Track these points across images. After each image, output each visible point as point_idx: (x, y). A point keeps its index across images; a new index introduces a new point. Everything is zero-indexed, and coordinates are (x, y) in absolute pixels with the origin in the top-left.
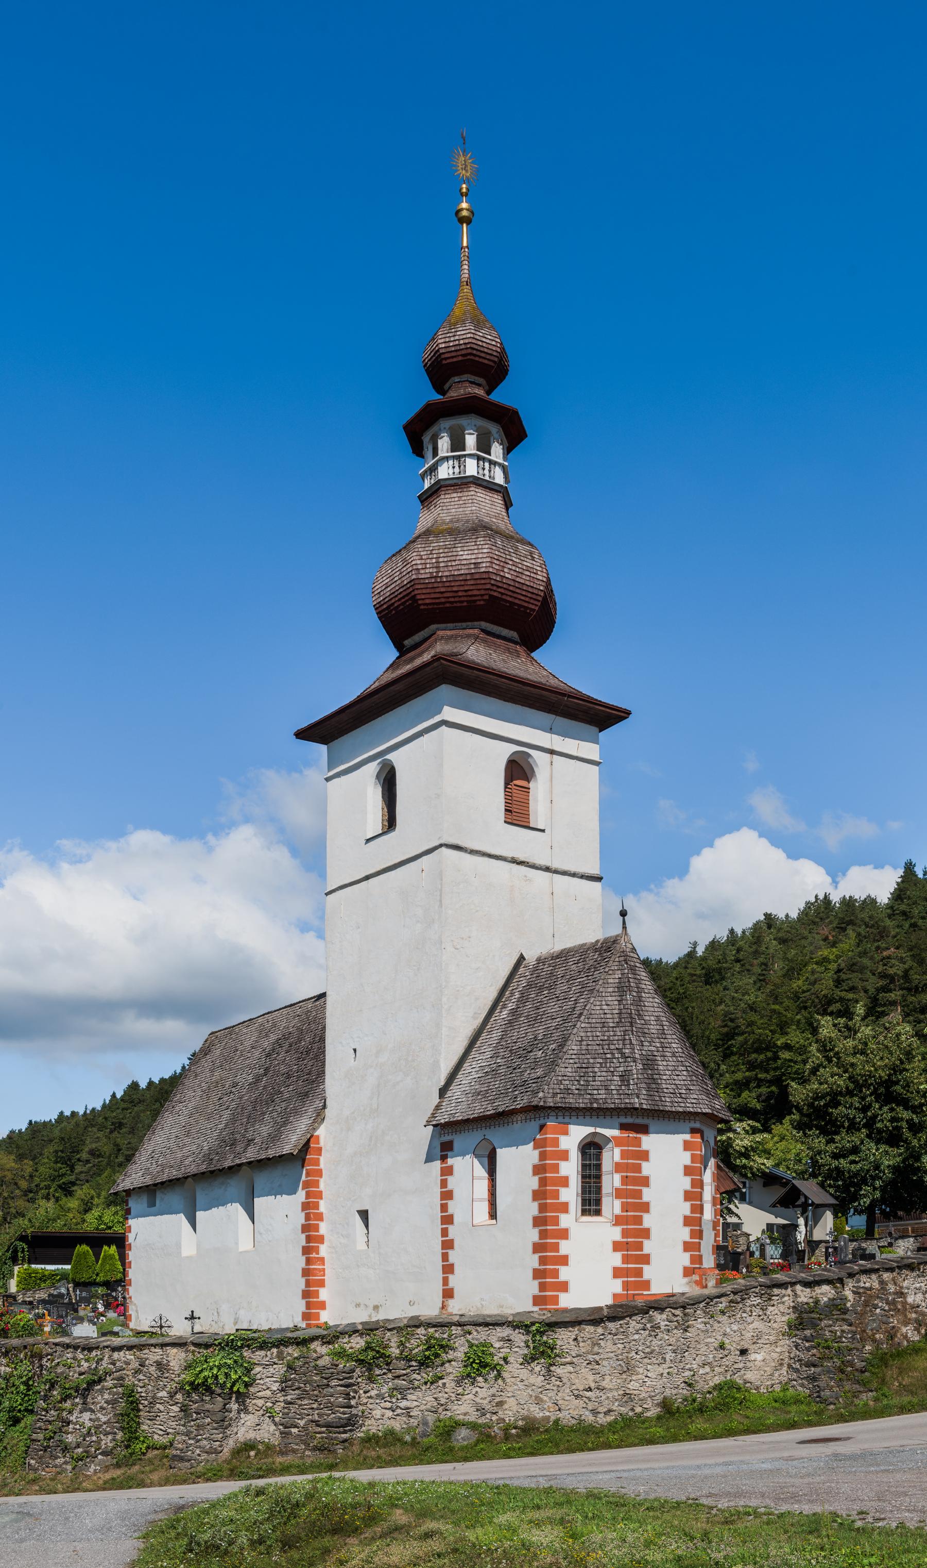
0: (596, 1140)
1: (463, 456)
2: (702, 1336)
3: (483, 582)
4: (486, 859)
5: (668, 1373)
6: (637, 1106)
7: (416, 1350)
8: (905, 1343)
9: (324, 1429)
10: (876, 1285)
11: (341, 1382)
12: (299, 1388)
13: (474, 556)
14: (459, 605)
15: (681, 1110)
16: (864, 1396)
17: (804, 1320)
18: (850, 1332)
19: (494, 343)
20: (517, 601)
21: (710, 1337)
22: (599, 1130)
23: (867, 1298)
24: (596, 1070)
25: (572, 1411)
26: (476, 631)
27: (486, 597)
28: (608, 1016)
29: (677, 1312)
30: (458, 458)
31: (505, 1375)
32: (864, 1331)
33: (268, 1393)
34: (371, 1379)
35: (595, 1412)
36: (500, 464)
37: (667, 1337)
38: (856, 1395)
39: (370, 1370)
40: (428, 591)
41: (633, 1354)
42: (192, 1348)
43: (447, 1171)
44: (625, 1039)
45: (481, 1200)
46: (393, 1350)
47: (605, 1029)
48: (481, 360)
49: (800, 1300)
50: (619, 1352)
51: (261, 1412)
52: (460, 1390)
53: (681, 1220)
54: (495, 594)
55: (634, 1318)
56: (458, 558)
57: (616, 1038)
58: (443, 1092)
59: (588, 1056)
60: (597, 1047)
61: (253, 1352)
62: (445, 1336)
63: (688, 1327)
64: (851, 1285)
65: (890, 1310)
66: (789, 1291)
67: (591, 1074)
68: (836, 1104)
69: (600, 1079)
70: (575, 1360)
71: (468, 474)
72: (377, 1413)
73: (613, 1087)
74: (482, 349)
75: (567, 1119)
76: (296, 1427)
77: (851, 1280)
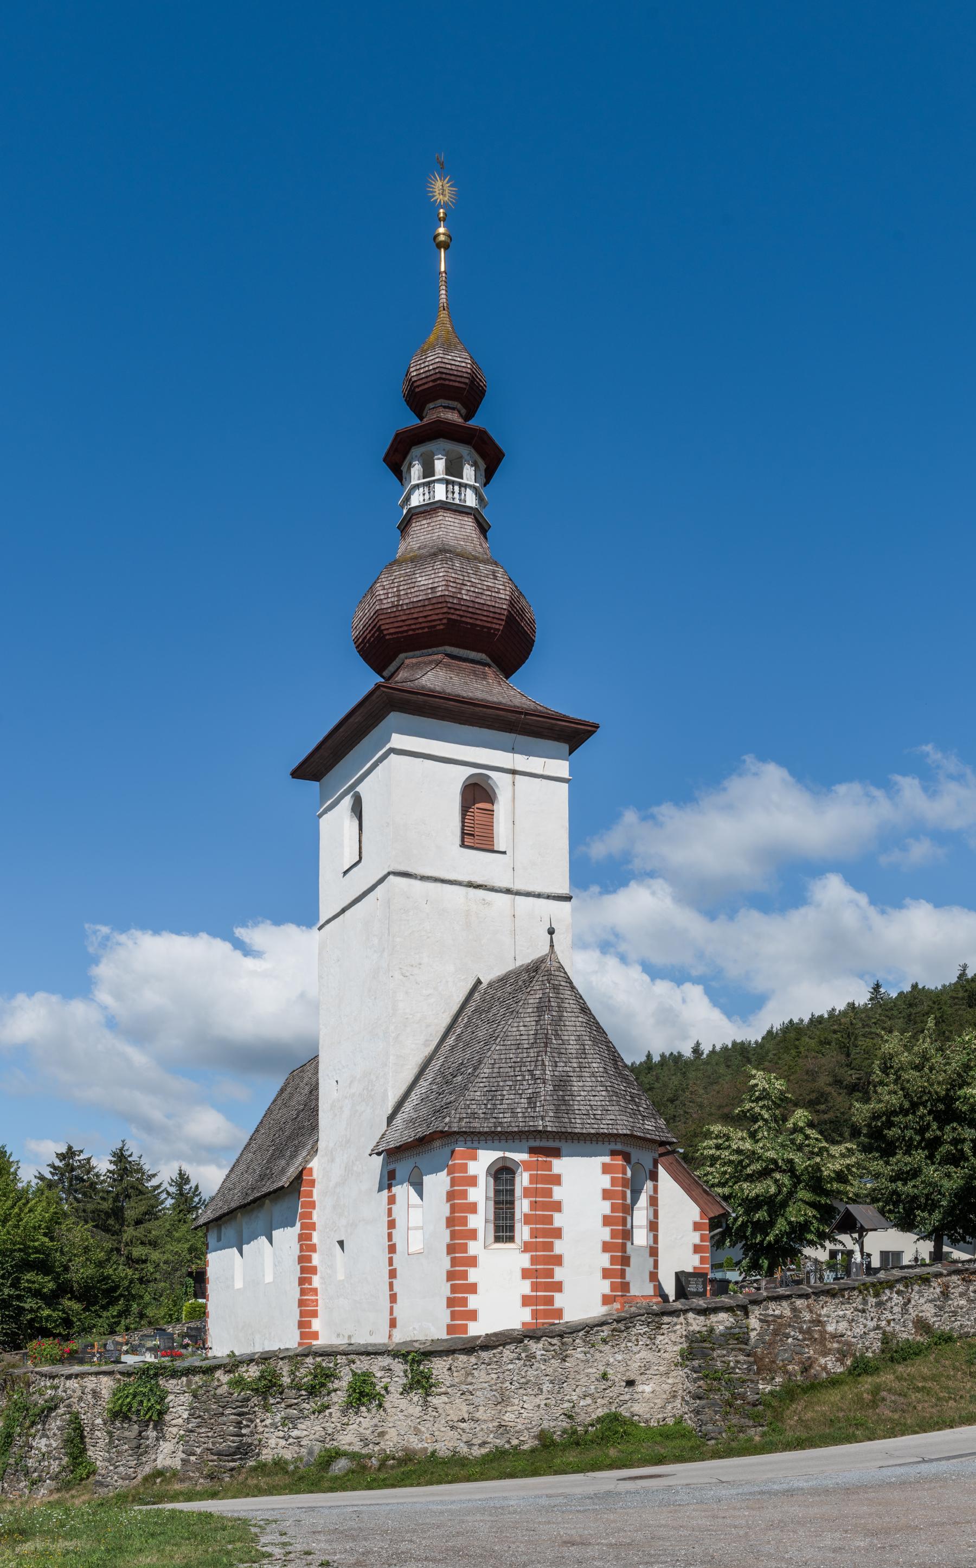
0: (509, 1164)
1: (436, 483)
2: (582, 1366)
3: (440, 606)
4: (439, 885)
5: (546, 1405)
6: (541, 1128)
7: (306, 1380)
8: (824, 1375)
9: (215, 1457)
10: (787, 1313)
11: (234, 1411)
12: (200, 1416)
13: (431, 581)
14: (420, 631)
15: (593, 1131)
16: (752, 1432)
17: (697, 1350)
18: (745, 1362)
19: (463, 364)
20: (478, 622)
21: (591, 1367)
22: (508, 1154)
23: (777, 1328)
24: (505, 1093)
25: (446, 1442)
26: (440, 657)
27: (445, 621)
28: (524, 1037)
29: (554, 1341)
30: (428, 484)
31: (387, 1405)
32: (774, 1362)
33: (180, 1421)
34: (266, 1408)
35: (469, 1444)
36: (470, 486)
37: (543, 1367)
38: (742, 1429)
39: (265, 1399)
40: (391, 620)
41: (508, 1384)
42: (119, 1376)
43: (392, 1200)
44: (537, 1061)
45: (640, 1227)
46: (284, 1379)
47: (519, 1051)
48: (451, 383)
49: (691, 1328)
50: (493, 1382)
51: (176, 1440)
52: (346, 1420)
53: (600, 1246)
54: (453, 617)
55: (507, 1347)
56: (417, 584)
57: (529, 1059)
58: (391, 1119)
59: (499, 1079)
60: (509, 1070)
61: (167, 1381)
62: (331, 1365)
63: (566, 1356)
64: (757, 1313)
65: (804, 1339)
66: (682, 1319)
67: (500, 1098)
68: (890, 1124)
69: (507, 1102)
70: (449, 1390)
71: (436, 499)
72: (272, 1442)
73: (519, 1110)
74: (451, 372)
75: (476, 1144)
76: (194, 1455)
77: (757, 1308)
